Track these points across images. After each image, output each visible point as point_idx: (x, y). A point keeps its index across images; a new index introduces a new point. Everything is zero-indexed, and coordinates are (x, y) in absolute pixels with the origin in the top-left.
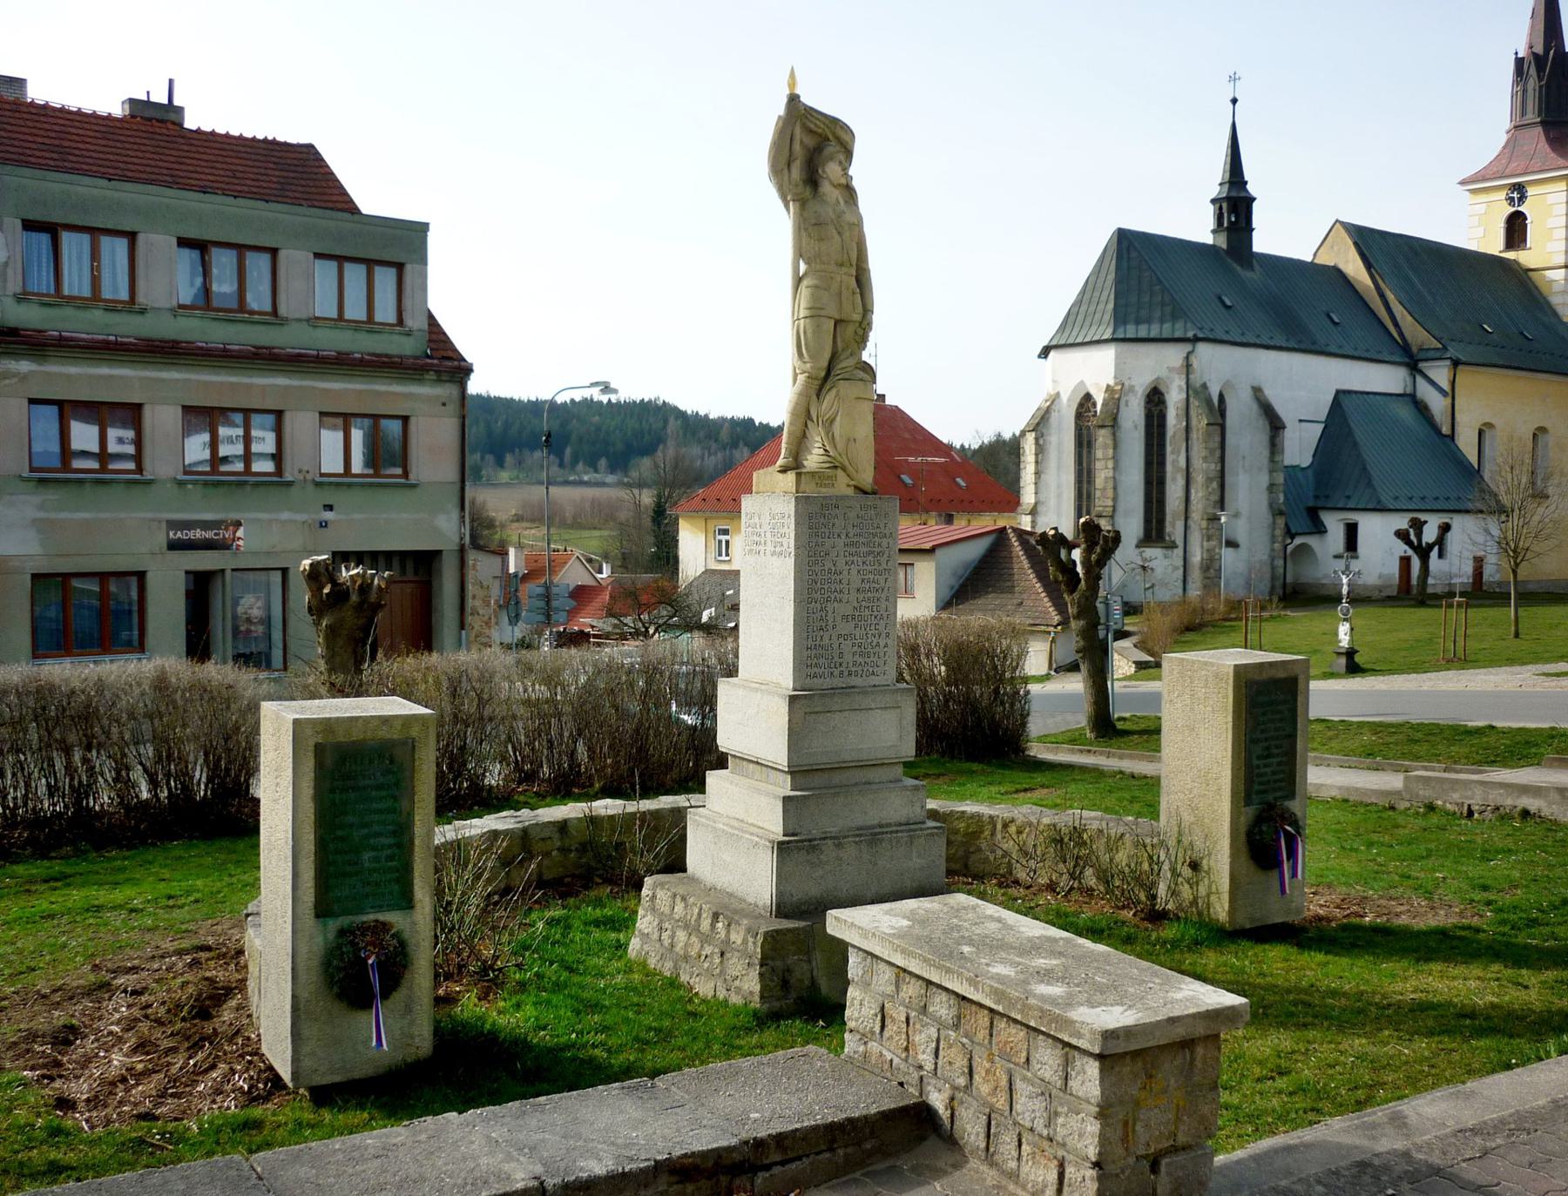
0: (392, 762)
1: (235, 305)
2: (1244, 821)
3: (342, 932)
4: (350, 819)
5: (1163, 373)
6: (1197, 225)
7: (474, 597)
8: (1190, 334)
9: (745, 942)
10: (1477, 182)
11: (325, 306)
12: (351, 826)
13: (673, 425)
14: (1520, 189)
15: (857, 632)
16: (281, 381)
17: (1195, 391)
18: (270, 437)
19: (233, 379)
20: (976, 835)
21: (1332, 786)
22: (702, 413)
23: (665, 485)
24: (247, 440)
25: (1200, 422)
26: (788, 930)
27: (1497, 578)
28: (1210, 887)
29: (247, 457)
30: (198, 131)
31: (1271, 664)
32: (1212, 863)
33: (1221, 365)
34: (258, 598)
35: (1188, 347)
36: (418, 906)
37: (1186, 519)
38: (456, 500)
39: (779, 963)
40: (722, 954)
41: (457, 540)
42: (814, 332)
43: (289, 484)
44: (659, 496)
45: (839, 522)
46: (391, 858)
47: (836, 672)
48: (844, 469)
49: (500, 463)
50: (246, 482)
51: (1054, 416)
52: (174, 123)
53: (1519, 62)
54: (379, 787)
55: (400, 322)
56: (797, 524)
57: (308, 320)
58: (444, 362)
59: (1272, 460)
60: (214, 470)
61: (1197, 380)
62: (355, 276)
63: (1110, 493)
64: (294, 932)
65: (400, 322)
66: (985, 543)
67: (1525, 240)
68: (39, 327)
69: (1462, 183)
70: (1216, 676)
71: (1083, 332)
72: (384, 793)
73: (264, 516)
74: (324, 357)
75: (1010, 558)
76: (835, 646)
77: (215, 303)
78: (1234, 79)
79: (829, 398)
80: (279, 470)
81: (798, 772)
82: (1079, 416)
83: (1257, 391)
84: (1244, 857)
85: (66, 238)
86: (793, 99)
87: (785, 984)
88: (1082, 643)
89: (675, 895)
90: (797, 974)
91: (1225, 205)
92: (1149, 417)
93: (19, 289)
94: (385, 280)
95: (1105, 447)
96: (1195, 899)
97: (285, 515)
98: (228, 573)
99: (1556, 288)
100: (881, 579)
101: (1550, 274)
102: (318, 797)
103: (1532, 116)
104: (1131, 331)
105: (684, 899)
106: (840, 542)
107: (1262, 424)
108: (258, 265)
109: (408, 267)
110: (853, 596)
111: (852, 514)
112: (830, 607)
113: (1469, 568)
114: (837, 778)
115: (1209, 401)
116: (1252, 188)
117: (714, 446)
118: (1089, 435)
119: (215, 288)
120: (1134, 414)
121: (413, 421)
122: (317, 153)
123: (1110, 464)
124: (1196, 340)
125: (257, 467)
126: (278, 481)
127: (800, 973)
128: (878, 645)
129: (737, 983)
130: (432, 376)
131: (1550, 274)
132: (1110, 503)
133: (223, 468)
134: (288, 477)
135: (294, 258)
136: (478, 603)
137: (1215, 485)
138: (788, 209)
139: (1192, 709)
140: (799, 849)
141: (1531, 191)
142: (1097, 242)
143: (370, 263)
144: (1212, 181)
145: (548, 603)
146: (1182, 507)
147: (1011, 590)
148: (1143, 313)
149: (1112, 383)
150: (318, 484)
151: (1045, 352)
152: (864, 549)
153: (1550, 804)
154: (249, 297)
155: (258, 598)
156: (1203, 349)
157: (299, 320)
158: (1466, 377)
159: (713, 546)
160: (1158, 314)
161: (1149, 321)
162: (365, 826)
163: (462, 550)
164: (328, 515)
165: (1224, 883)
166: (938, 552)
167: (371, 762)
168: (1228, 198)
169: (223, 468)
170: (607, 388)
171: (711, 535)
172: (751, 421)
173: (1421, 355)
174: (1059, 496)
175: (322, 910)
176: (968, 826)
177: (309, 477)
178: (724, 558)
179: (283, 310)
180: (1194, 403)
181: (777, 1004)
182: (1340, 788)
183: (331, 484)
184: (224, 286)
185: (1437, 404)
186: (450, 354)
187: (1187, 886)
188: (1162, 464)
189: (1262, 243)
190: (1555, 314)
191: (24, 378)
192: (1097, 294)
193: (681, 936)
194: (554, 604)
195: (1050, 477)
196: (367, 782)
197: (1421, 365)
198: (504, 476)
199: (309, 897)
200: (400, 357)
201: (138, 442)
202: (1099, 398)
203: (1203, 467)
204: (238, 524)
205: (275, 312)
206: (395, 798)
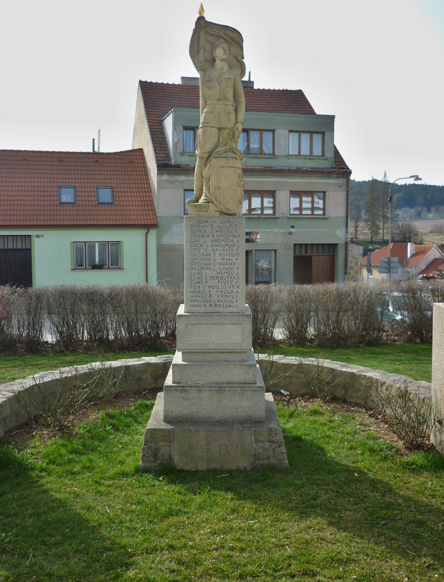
1: (259, 152)
7: (351, 262)
11: (293, 150)
16: (275, 179)
18: (321, 202)
19: (257, 179)
20: (370, 388)
24: (313, 202)
29: (313, 209)
30: (258, 89)
34: (266, 261)
38: (344, 224)
39: (154, 445)
41: (344, 239)
43: (278, 218)
47: (208, 305)
48: (212, 202)
49: (429, 211)
50: (262, 218)
52: (250, 87)
55: (323, 155)
57: (286, 156)
58: (340, 169)
60: (250, 213)
62: (305, 138)
65: (323, 155)
68: (188, 164)
73: (268, 230)
74: (291, 170)
76: (207, 291)
77: (251, 152)
80: (324, 214)
85: (251, 133)
87: (155, 455)
90: (162, 452)
93: (181, 151)
94: (317, 139)
97: (276, 230)
98: (254, 251)
100: (234, 259)
108: (268, 136)
109: (326, 134)
110: (217, 267)
112: (203, 272)
114: (208, 357)
119: (251, 146)
121: (327, 193)
122: (303, 93)
125: (266, 212)
126: (324, 217)
127: (164, 450)
128: (232, 292)
130: (334, 175)
133: (253, 213)
134: (277, 215)
135: (281, 133)
136: (353, 265)
140: (176, 391)
143: (311, 133)
145: (389, 265)
150: (288, 218)
154: (264, 148)
155: (266, 261)
157: (282, 156)
163: (346, 244)
164: (292, 230)
169: (253, 213)
170: (417, 178)
176: (367, 383)
177: (285, 216)
179: (276, 153)
181: (148, 465)
183: (293, 218)
184: (254, 145)
186: (344, 166)
191: (182, 182)
194: (392, 265)
198: (431, 215)
200: (322, 168)
201: (274, 203)
204: (257, 233)
205: (273, 154)
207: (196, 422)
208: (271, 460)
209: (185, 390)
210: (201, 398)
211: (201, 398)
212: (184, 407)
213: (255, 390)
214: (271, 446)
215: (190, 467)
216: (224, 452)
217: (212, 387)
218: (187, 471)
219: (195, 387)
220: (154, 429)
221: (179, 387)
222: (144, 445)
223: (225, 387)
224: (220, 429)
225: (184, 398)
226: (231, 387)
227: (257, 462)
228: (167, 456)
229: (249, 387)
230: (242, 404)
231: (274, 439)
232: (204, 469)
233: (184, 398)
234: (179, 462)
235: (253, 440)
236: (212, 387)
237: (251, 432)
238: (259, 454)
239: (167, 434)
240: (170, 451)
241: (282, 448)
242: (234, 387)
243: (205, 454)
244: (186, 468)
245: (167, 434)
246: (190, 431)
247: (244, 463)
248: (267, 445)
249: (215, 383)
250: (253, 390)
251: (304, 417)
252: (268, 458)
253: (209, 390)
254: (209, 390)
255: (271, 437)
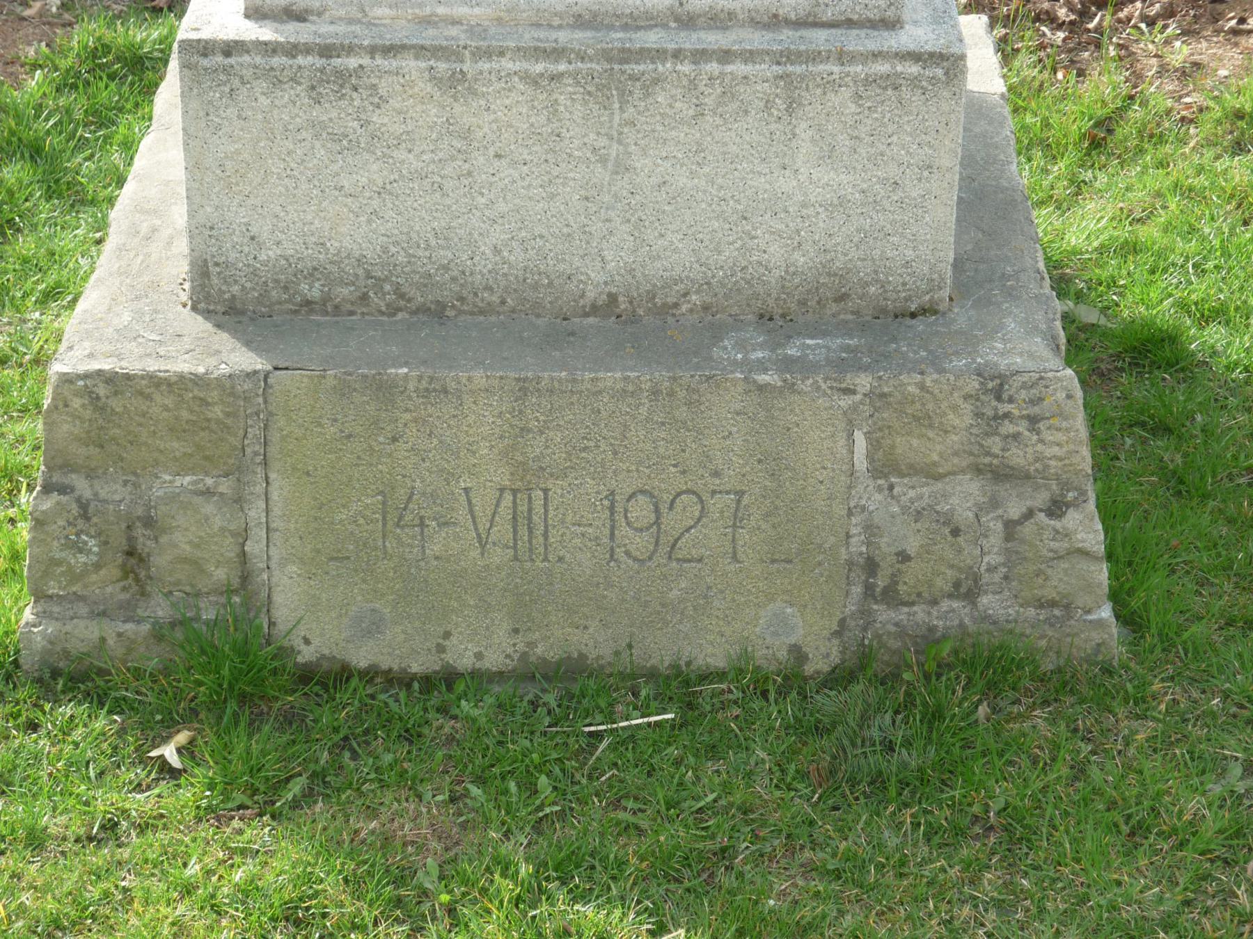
39: (114, 492)
127: (194, 538)
140: (276, 80)
181: (85, 633)
207: (437, 313)
208: (985, 600)
209: (342, 76)
210: (467, 135)
211: (467, 135)
212: (339, 203)
213: (892, 82)
214: (994, 503)
215: (398, 647)
216: (640, 543)
217: (557, 53)
218: (368, 675)
219: (420, 51)
220: (110, 378)
221: (292, 50)
222: (47, 489)
223: (659, 54)
224: (611, 378)
225: (336, 138)
226: (700, 56)
227: (885, 616)
228: (220, 574)
229: (842, 57)
230: (786, 183)
231: (1018, 457)
232: (494, 661)
233: (336, 138)
234: (312, 616)
235: (861, 462)
236: (557, 53)
237: (845, 402)
238: (904, 557)
239: (217, 412)
240: (243, 535)
241: (1072, 519)
242: (726, 56)
243: (498, 556)
244: (361, 658)
245: (217, 412)
246: (385, 390)
247: (795, 624)
248: (964, 496)
249: (580, 22)
250: (869, 81)
251: (1189, 160)
252: (967, 588)
253: (526, 77)
254: (526, 77)
255: (995, 444)
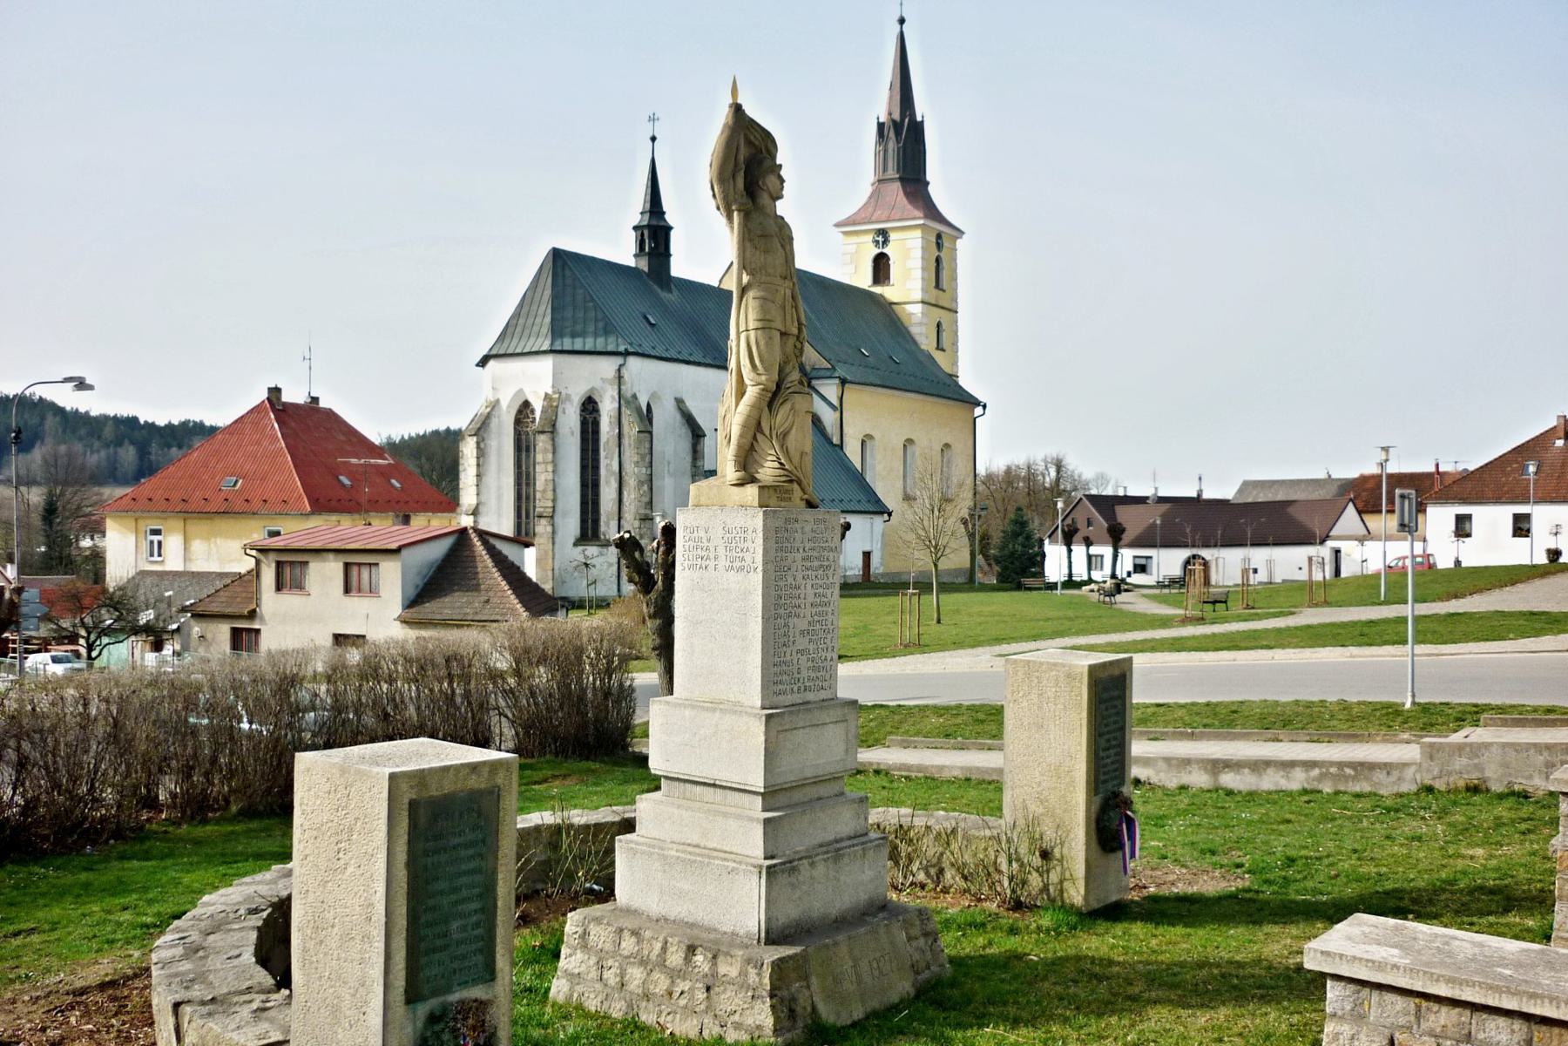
0: (479, 815)
2: (1094, 808)
3: (433, 1019)
4: (442, 885)
5: (598, 384)
6: (623, 251)
8: (622, 349)
9: (743, 973)
10: (848, 225)
12: (441, 893)
13: (51, 422)
14: (883, 233)
15: (811, 647)
17: (625, 400)
21: (953, 767)
22: (82, 410)
23: (56, 483)
25: (631, 429)
26: (790, 957)
27: (881, 570)
28: (1063, 873)
31: (1111, 663)
32: (1065, 851)
33: (651, 378)
35: (619, 360)
36: (499, 975)
37: (619, 519)
39: (785, 993)
40: (708, 989)
42: (767, 344)
44: (50, 494)
45: (798, 536)
46: (477, 925)
51: (494, 422)
53: (881, 126)
54: (467, 846)
56: (765, 539)
59: (694, 465)
61: (628, 391)
63: (550, 495)
64: (385, 1024)
66: (447, 543)
67: (888, 278)
69: (837, 225)
70: (1068, 676)
71: (522, 343)
72: (471, 852)
75: (473, 558)
78: (653, 119)
79: (783, 412)
81: (771, 796)
82: (518, 422)
83: (679, 402)
84: (1094, 844)
86: (737, 109)
88: (658, 641)
89: (621, 930)
91: (646, 233)
92: (584, 423)
95: (545, 451)
96: (1045, 888)
99: (915, 320)
101: (909, 308)
102: (411, 863)
103: (892, 173)
104: (567, 344)
105: (635, 933)
106: (799, 556)
107: (685, 432)
111: (808, 529)
112: (792, 621)
113: (859, 562)
114: (797, 796)
115: (639, 410)
116: (670, 218)
117: (97, 444)
118: (528, 441)
120: (570, 421)
123: (550, 468)
124: (627, 354)
129: (736, 1017)
131: (909, 308)
132: (550, 504)
137: (645, 487)
138: (730, 217)
139: (1040, 708)
141: (893, 236)
142: (536, 257)
144: (634, 211)
146: (616, 509)
147: (476, 588)
148: (579, 328)
149: (550, 391)
151: (483, 362)
152: (816, 563)
153: (1158, 772)
156: (633, 362)
158: (852, 394)
159: (145, 546)
160: (591, 328)
161: (583, 334)
162: (456, 890)
165: (1079, 869)
166: (404, 552)
167: (461, 815)
168: (649, 226)
171: (141, 536)
172: (135, 419)
173: (814, 374)
174: (499, 497)
175: (412, 997)
178: (156, 558)
180: (626, 412)
181: (788, 1036)
182: (962, 768)
185: (829, 417)
187: (1035, 874)
188: (596, 468)
189: (680, 268)
190: (915, 342)
192: (534, 307)
193: (636, 974)
195: (490, 479)
196: (456, 841)
197: (814, 382)
199: (400, 982)
202: (538, 405)
203: (633, 472)
206: (481, 856)
